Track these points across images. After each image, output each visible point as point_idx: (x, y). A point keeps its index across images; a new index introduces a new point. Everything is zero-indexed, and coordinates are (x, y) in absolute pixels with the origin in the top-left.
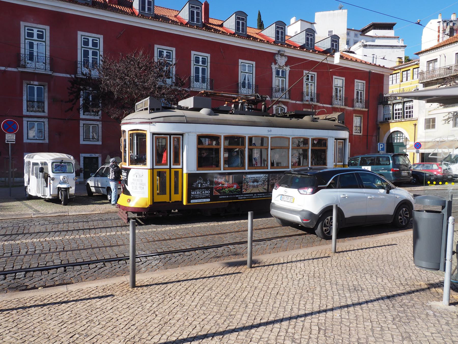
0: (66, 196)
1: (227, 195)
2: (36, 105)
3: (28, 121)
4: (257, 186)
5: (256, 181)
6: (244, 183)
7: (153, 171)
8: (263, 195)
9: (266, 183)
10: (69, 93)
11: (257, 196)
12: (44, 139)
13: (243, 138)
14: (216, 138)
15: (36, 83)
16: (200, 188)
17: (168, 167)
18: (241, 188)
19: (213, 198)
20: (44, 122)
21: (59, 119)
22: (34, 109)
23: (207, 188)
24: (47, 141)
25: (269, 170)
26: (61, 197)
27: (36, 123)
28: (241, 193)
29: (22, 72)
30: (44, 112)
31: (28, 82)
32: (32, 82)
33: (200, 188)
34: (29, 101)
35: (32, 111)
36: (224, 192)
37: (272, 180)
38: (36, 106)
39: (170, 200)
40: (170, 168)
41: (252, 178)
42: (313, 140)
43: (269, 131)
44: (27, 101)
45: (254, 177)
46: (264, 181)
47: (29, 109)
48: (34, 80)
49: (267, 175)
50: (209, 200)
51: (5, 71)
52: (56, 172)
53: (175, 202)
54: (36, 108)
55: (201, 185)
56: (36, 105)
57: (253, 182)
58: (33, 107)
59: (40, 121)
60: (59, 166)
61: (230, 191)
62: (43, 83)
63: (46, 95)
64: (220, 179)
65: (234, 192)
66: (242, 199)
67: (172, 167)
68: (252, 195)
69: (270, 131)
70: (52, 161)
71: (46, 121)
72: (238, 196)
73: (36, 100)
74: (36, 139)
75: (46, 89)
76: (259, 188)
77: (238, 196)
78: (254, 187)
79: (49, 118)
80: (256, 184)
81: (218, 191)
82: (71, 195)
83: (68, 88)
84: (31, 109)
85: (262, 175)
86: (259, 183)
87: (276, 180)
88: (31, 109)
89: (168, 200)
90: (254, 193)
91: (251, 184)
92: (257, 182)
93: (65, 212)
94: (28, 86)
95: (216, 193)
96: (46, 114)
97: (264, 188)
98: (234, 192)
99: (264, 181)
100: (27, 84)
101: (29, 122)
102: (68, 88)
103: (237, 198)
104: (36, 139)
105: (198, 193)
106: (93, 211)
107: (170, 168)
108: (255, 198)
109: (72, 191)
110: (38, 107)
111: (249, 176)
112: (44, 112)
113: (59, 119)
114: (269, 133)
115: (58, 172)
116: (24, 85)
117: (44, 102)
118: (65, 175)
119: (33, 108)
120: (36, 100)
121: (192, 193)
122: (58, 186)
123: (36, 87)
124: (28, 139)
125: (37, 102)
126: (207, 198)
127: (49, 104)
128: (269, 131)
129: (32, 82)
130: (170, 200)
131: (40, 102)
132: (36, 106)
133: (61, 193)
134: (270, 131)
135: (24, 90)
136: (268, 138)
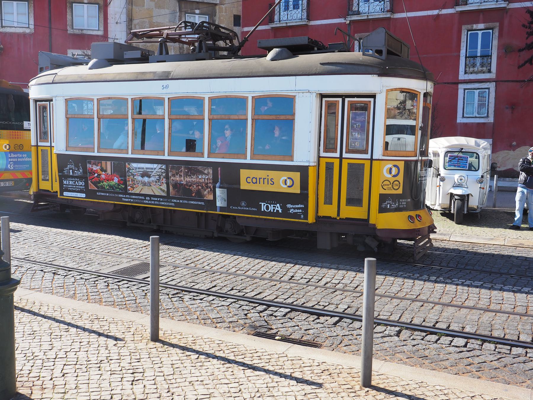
0: (460, 210)
1: (106, 192)
2: (478, 61)
3: (465, 89)
4: (149, 184)
5: (145, 174)
6: (129, 176)
7: (37, 148)
8: (159, 201)
9: (164, 181)
10: (527, 33)
11: (151, 200)
12: (488, 116)
13: (244, 100)
14: (197, 102)
15: (481, 26)
16: (72, 177)
17: (338, 155)
18: (125, 183)
19: (90, 193)
20: (489, 89)
21: (513, 81)
22: (476, 69)
23: (80, 178)
24: (491, 120)
25: (166, 157)
26: (454, 210)
27: (477, 92)
28: (125, 191)
29: (462, 12)
30: (490, 71)
31: (469, 27)
32: (475, 27)
33: (72, 177)
34: (469, 57)
35: (471, 73)
36: (102, 187)
37: (174, 175)
38: (478, 64)
39: (338, 214)
40: (341, 158)
41: (139, 168)
42: (211, 99)
43: (164, 87)
44: (466, 57)
45: (143, 168)
46: (160, 176)
47: (468, 69)
48: (477, 22)
49: (164, 167)
50: (83, 195)
51: (438, 16)
52: (449, 168)
53: (347, 219)
54: (478, 67)
55: (73, 172)
56: (478, 61)
57: (143, 176)
58: (474, 65)
59: (483, 87)
60: (455, 157)
61: (111, 187)
62: (490, 25)
63: (495, 43)
64: (94, 166)
65: (116, 188)
66: (130, 202)
67: (345, 155)
68: (143, 198)
69: (167, 87)
70: (446, 150)
71: (492, 86)
72: (121, 196)
73: (479, 54)
74: (476, 117)
75: (496, 34)
76: (153, 187)
77: (121, 196)
78: (144, 184)
79: (497, 81)
80: (146, 179)
81: (95, 184)
82: (470, 209)
83: (524, 26)
84: (471, 69)
85: (155, 166)
86: (152, 179)
87: (181, 176)
88: (471, 69)
89: (334, 214)
90: (145, 195)
91: (140, 178)
92: (149, 176)
93: (445, 235)
94: (469, 32)
95: (92, 187)
96: (493, 76)
97: (161, 189)
98: (116, 188)
99: (160, 176)
100: (468, 31)
101: (466, 91)
102: (524, 26)
103: (120, 199)
104: (476, 117)
105: (71, 183)
106: (492, 239)
107: (341, 158)
108: (147, 204)
109: (474, 203)
110: (482, 65)
111: (134, 165)
112: (490, 71)
113: (513, 81)
114: (165, 91)
115: (452, 168)
116: (463, 32)
117: (491, 56)
118: (464, 173)
119: (474, 67)
120: (479, 54)
121: (65, 182)
122: (450, 191)
123: (480, 33)
124: (463, 117)
125: (480, 56)
126: (81, 191)
127: (499, 58)
128: (164, 87)
129: (475, 27)
130: (338, 214)
131: (486, 56)
132: (478, 64)
133: (454, 202)
134: (167, 87)
135: (462, 40)
136: (202, 100)
